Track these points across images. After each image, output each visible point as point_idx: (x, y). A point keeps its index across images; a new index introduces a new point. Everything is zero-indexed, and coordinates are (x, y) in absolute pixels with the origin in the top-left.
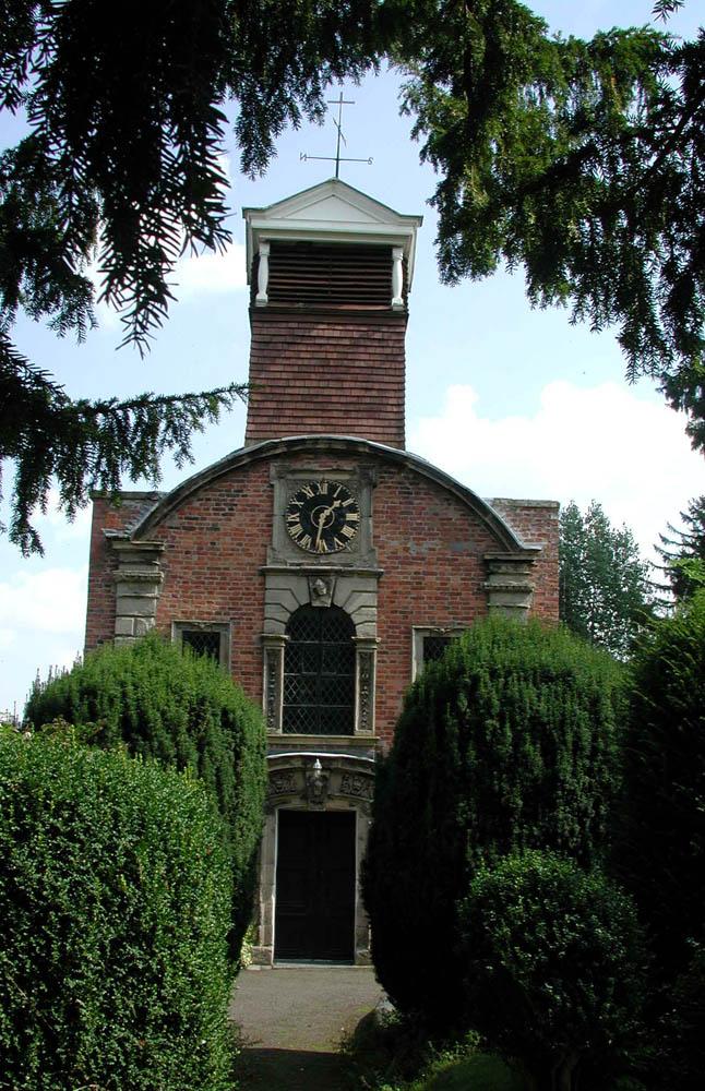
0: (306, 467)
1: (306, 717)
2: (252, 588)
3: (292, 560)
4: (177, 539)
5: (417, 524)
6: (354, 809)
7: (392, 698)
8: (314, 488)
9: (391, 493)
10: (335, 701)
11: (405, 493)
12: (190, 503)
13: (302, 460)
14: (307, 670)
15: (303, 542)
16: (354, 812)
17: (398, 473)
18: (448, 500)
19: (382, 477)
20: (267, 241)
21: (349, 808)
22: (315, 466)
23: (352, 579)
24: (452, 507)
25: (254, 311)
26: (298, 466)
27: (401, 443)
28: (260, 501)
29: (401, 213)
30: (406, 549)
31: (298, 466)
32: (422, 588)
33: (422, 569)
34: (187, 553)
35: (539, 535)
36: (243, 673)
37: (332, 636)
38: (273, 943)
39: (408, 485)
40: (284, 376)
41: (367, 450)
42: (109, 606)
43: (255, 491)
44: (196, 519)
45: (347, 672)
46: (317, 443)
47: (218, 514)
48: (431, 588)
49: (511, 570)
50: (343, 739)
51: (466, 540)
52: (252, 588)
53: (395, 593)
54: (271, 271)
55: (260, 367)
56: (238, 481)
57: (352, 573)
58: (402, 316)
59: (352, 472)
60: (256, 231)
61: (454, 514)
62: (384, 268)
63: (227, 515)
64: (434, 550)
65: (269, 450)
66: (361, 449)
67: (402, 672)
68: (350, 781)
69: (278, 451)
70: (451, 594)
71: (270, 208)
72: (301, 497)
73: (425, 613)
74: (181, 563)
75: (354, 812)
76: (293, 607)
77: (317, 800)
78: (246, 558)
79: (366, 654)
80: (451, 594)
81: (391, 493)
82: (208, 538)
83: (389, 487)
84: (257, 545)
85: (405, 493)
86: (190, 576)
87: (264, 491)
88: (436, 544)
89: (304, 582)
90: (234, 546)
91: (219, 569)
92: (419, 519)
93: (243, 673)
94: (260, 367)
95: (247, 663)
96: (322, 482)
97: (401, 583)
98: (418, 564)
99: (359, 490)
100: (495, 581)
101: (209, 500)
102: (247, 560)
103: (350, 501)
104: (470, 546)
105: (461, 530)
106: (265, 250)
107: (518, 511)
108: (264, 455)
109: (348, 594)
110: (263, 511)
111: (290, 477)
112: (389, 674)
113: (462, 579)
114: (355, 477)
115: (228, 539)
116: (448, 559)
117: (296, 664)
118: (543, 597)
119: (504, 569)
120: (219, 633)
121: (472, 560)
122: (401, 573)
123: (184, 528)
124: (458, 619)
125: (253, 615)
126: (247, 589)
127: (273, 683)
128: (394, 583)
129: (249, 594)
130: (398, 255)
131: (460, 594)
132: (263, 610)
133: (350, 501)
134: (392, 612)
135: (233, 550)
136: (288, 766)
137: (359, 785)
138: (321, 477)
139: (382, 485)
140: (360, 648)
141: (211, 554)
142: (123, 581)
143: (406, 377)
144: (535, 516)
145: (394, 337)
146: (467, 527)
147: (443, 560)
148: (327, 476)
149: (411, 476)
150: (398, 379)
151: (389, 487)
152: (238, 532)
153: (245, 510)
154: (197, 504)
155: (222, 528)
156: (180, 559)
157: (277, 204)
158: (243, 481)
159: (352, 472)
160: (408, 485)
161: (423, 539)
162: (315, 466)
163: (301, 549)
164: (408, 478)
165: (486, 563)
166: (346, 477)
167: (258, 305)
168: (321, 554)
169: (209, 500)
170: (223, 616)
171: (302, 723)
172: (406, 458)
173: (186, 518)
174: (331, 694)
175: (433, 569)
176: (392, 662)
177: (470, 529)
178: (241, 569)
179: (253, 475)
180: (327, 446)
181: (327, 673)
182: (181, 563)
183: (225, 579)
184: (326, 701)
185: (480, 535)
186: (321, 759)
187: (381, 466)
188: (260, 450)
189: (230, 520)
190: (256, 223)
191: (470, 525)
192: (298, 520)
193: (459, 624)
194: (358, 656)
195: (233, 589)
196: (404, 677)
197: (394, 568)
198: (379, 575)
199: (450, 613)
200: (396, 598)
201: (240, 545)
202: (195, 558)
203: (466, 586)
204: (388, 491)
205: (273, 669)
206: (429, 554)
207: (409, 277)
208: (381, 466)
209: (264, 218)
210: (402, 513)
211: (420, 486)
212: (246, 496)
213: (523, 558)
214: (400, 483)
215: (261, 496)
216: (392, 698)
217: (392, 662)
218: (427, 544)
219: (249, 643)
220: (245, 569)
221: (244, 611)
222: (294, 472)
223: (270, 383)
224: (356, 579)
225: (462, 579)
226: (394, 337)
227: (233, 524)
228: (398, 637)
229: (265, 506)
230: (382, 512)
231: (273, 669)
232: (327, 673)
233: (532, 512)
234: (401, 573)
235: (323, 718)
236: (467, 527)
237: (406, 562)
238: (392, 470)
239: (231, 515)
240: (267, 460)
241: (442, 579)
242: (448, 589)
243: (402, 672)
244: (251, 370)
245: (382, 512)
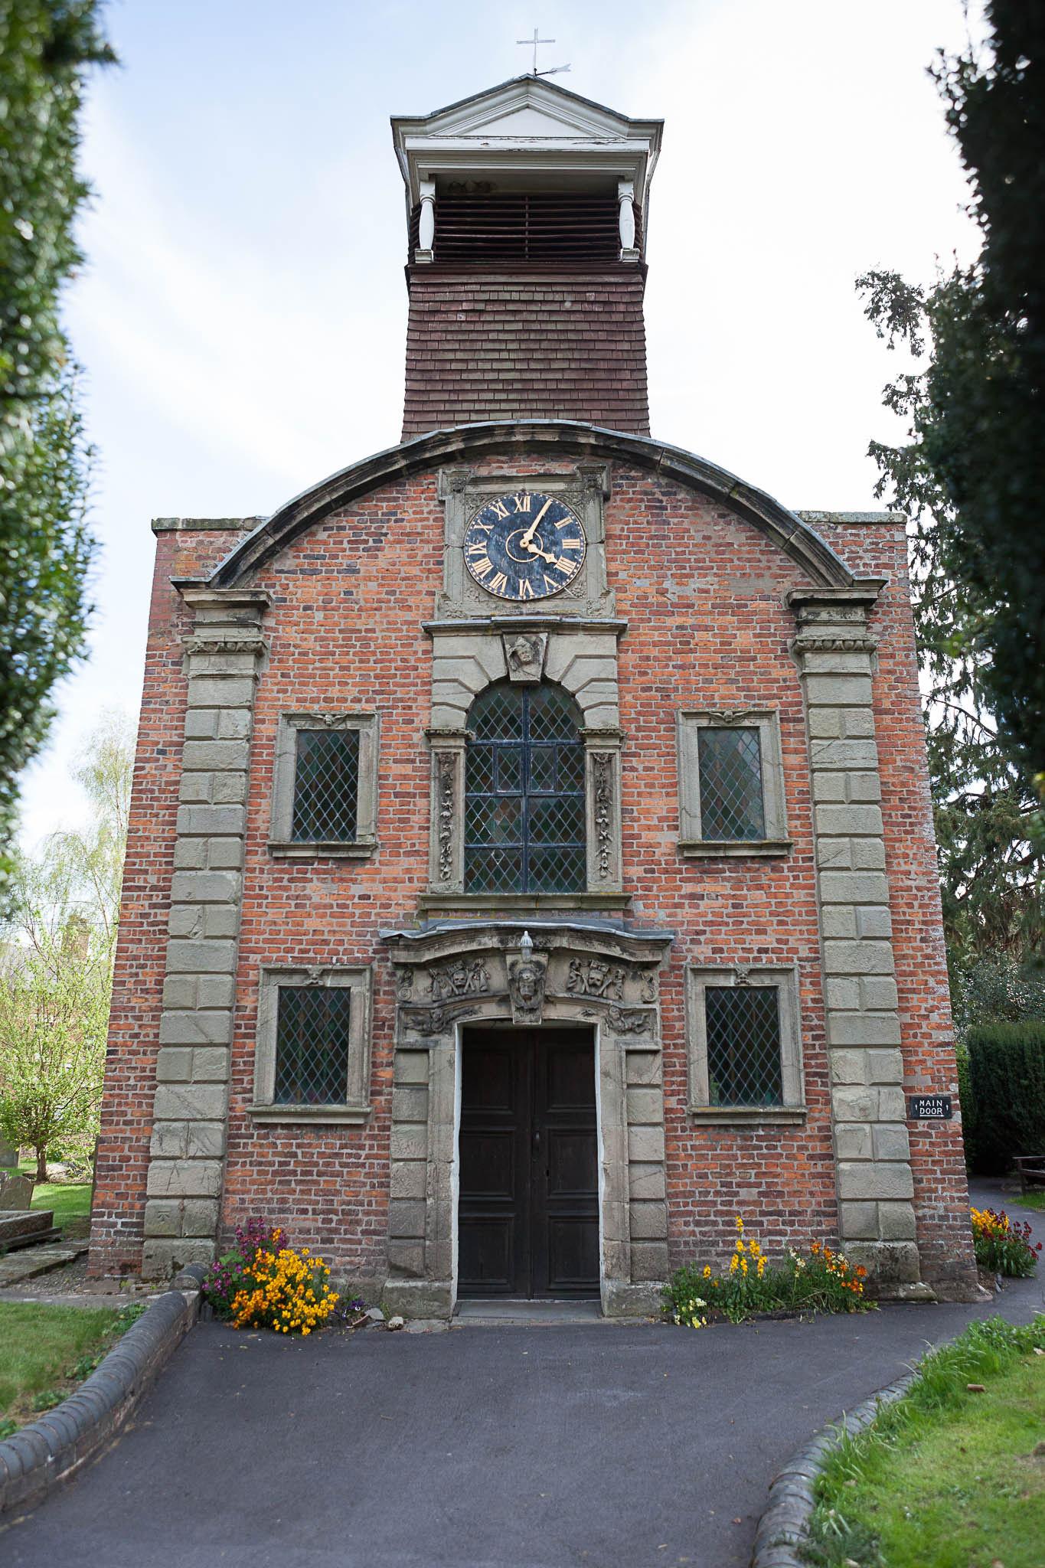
0: (496, 473)
1: (504, 864)
2: (412, 658)
3: (476, 610)
4: (291, 588)
5: (677, 553)
6: (592, 1020)
7: (649, 828)
8: (510, 504)
9: (632, 509)
10: (553, 836)
11: (656, 508)
12: (313, 534)
13: (489, 464)
14: (505, 786)
15: (494, 584)
16: (593, 1027)
17: (643, 479)
18: (721, 516)
19: (615, 486)
20: (433, 177)
21: (582, 1018)
22: (507, 471)
23: (575, 638)
24: (732, 528)
25: (410, 271)
26: (484, 472)
27: (640, 416)
28: (423, 527)
29: (633, 115)
30: (663, 592)
31: (484, 472)
32: (691, 651)
33: (690, 621)
34: (306, 608)
35: (877, 566)
36: (397, 795)
37: (546, 730)
38: (455, 1273)
39: (658, 496)
40: (460, 355)
41: (592, 441)
42: (176, 695)
43: (415, 513)
44: (323, 557)
45: (572, 787)
46: (512, 434)
47: (357, 549)
48: (706, 650)
49: (837, 618)
50: (564, 899)
51: (760, 576)
52: (412, 658)
53: (648, 658)
54: (437, 223)
55: (420, 327)
56: (388, 500)
57: (574, 628)
58: (640, 269)
59: (570, 478)
60: (414, 155)
61: (735, 534)
62: (611, 254)
63: (373, 552)
64: (707, 591)
65: (434, 448)
66: (582, 440)
67: (663, 786)
68: (584, 972)
69: (450, 449)
70: (740, 659)
71: (434, 117)
72: (489, 518)
73: (697, 690)
74: (297, 624)
75: (593, 1027)
76: (478, 684)
77: (528, 1004)
78: (400, 613)
79: (602, 756)
80: (740, 659)
81: (632, 509)
82: (339, 585)
83: (630, 500)
84: (419, 593)
85: (656, 508)
86: (311, 643)
87: (429, 513)
88: (710, 582)
89: (496, 643)
90: (384, 596)
91: (359, 631)
92: (680, 545)
93: (397, 795)
94: (420, 327)
95: (405, 777)
96: (523, 492)
97: (655, 644)
98: (682, 614)
99: (582, 503)
100: (809, 633)
101: (344, 528)
102: (409, 616)
103: (567, 521)
104: (766, 584)
105: (749, 560)
106: (428, 191)
107: (840, 530)
108: (428, 455)
109: (570, 659)
110: (428, 542)
111: (470, 489)
112: (643, 789)
113: (755, 636)
114: (575, 486)
115: (373, 586)
116: (731, 606)
117: (485, 778)
118: (891, 661)
119: (824, 616)
120: (358, 731)
121: (772, 606)
122: (655, 629)
123: (303, 572)
124: (752, 697)
125: (415, 700)
126: (404, 660)
127: (447, 808)
128: (642, 644)
129: (408, 668)
130: (625, 190)
131: (754, 659)
132: (429, 693)
133: (567, 521)
134: (644, 690)
135: (379, 601)
136: (474, 946)
137: (599, 976)
138: (520, 486)
139: (618, 497)
140: (594, 747)
141: (346, 609)
142: (200, 652)
143: (649, 392)
144: (867, 536)
145: (626, 298)
146: (758, 556)
147: (722, 607)
148: (528, 486)
149: (663, 481)
150: (638, 396)
151: (630, 500)
152: (387, 576)
153: (399, 542)
154: (322, 536)
155: (362, 569)
156: (295, 618)
157: (443, 111)
158: (396, 499)
159: (570, 478)
160: (658, 496)
161: (687, 576)
162: (507, 471)
163: (490, 594)
164: (659, 486)
165: (795, 605)
166: (561, 486)
167: (420, 260)
168: (523, 602)
169: (344, 528)
170: (364, 705)
171: (498, 874)
172: (656, 448)
173: (305, 557)
174: (546, 825)
175: (707, 620)
176: (646, 769)
177: (763, 558)
178: (394, 630)
179: (411, 490)
180: (528, 438)
181: (539, 790)
182: (297, 624)
183: (368, 646)
184: (539, 836)
185: (780, 568)
186: (534, 932)
187: (615, 468)
188: (422, 446)
189: (376, 557)
190: (411, 144)
191: (762, 552)
192: (484, 551)
193: (754, 705)
194: (588, 757)
195: (382, 661)
196: (668, 794)
197: (642, 620)
198: (620, 630)
199: (739, 689)
200: (648, 666)
201: (393, 593)
202: (319, 616)
203: (763, 648)
204: (627, 506)
205: (446, 783)
206: (700, 598)
207: (643, 213)
208: (615, 468)
209: (425, 135)
210: (651, 538)
211: (679, 497)
212: (402, 520)
213: (856, 595)
214: (646, 493)
215: (427, 519)
216: (649, 828)
217: (646, 769)
218: (696, 583)
219: (410, 746)
220: (401, 630)
221: (399, 695)
222: (476, 481)
223: (438, 366)
224: (581, 638)
225: (755, 636)
226: (626, 298)
227: (382, 562)
228: (655, 730)
229: (431, 534)
230: (620, 537)
231: (446, 783)
232: (539, 790)
233: (864, 531)
234: (655, 629)
235: (532, 864)
236: (758, 556)
237: (662, 611)
238: (633, 474)
239: (378, 549)
240: (430, 465)
241: (722, 635)
242: (735, 651)
243: (663, 786)
244: (405, 411)
245: (620, 537)
